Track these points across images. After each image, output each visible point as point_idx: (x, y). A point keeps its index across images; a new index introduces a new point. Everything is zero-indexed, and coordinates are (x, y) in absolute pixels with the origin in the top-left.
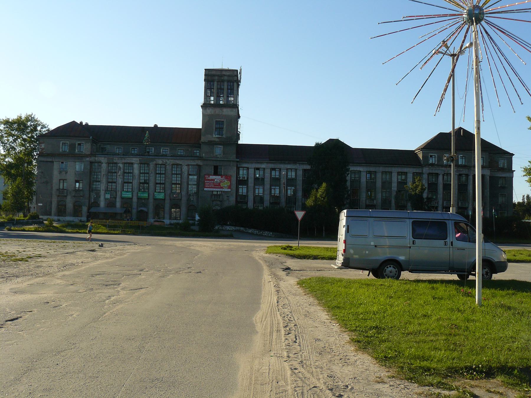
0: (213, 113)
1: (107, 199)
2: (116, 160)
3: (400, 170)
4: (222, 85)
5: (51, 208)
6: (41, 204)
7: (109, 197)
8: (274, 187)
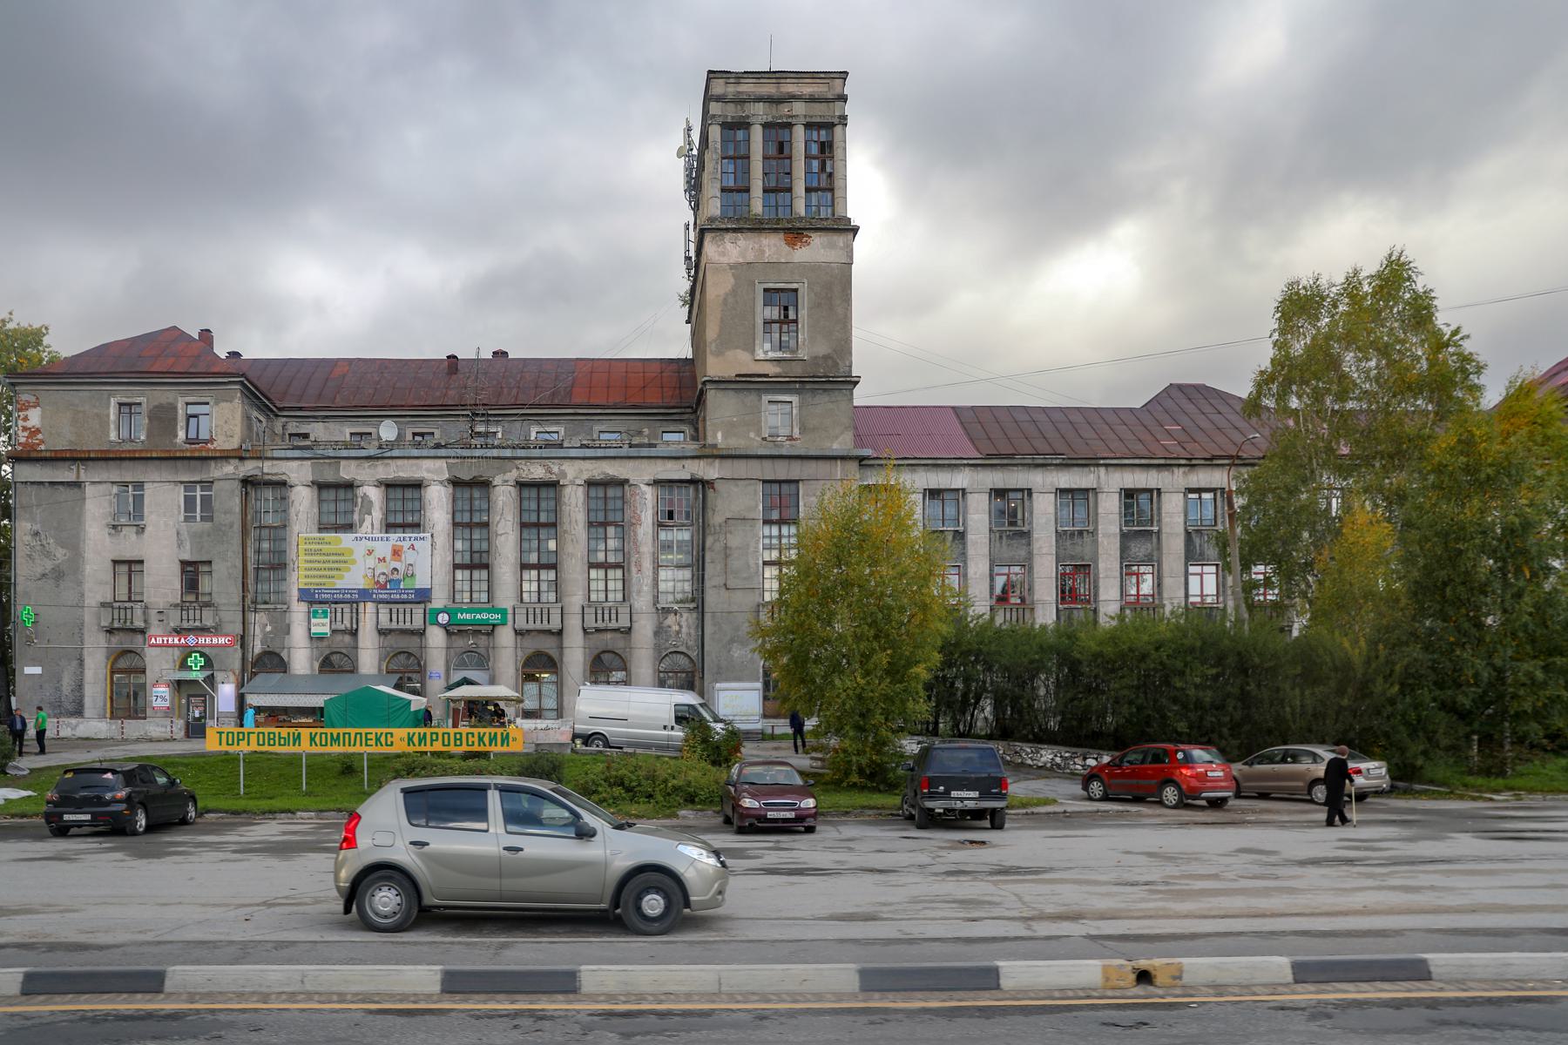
0: (750, 257)
1: (321, 638)
2: (348, 471)
3: (1067, 479)
4: (769, 150)
5: (79, 686)
6: (38, 670)
7: (326, 630)
8: (1197, 569)
